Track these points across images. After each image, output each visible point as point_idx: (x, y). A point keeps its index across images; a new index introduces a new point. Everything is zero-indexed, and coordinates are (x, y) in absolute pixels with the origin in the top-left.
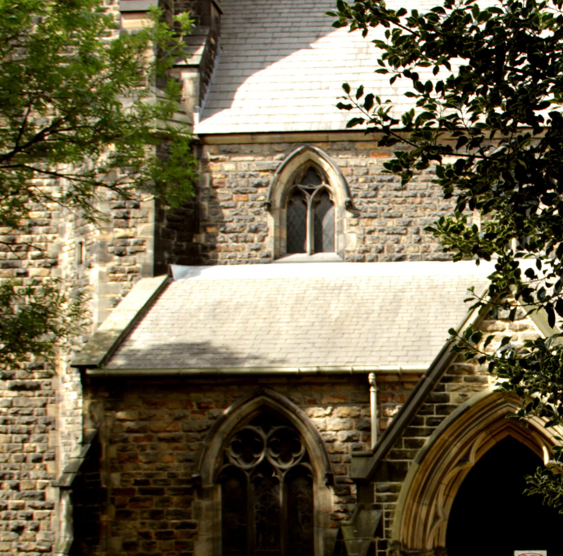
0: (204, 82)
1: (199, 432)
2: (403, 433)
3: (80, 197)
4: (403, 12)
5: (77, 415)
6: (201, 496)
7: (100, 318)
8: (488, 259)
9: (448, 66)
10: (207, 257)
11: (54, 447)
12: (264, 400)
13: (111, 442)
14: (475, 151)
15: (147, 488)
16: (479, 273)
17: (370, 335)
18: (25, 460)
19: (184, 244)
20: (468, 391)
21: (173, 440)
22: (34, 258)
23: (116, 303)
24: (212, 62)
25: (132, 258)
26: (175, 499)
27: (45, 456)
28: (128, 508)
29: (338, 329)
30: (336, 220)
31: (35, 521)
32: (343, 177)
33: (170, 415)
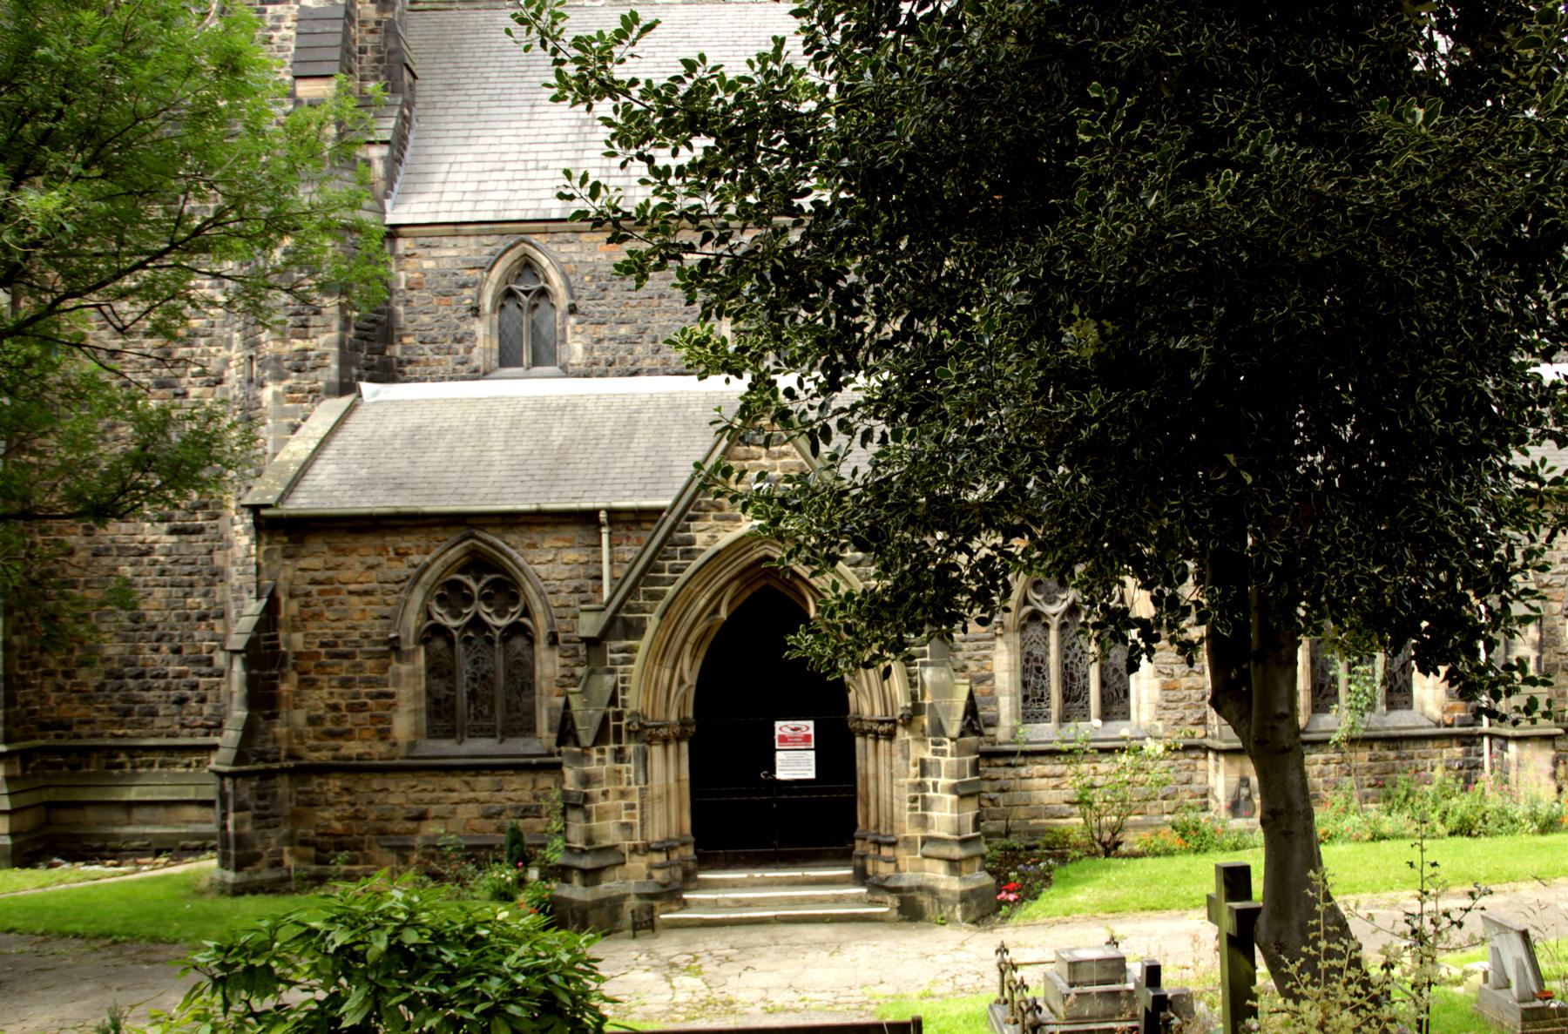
0: (394, 162)
3: (251, 299)
4: (634, 82)
6: (399, 660)
7: (275, 447)
8: (740, 376)
9: (690, 147)
10: (404, 373)
11: (222, 603)
13: (292, 596)
14: (722, 249)
15: (336, 651)
16: (731, 389)
18: (187, 618)
21: (366, 593)
22: (194, 376)
23: (295, 429)
24: (405, 138)
25: (313, 375)
26: (370, 663)
27: (212, 613)
28: (312, 675)
29: (562, 457)
30: (559, 327)
31: (201, 690)
32: (564, 275)
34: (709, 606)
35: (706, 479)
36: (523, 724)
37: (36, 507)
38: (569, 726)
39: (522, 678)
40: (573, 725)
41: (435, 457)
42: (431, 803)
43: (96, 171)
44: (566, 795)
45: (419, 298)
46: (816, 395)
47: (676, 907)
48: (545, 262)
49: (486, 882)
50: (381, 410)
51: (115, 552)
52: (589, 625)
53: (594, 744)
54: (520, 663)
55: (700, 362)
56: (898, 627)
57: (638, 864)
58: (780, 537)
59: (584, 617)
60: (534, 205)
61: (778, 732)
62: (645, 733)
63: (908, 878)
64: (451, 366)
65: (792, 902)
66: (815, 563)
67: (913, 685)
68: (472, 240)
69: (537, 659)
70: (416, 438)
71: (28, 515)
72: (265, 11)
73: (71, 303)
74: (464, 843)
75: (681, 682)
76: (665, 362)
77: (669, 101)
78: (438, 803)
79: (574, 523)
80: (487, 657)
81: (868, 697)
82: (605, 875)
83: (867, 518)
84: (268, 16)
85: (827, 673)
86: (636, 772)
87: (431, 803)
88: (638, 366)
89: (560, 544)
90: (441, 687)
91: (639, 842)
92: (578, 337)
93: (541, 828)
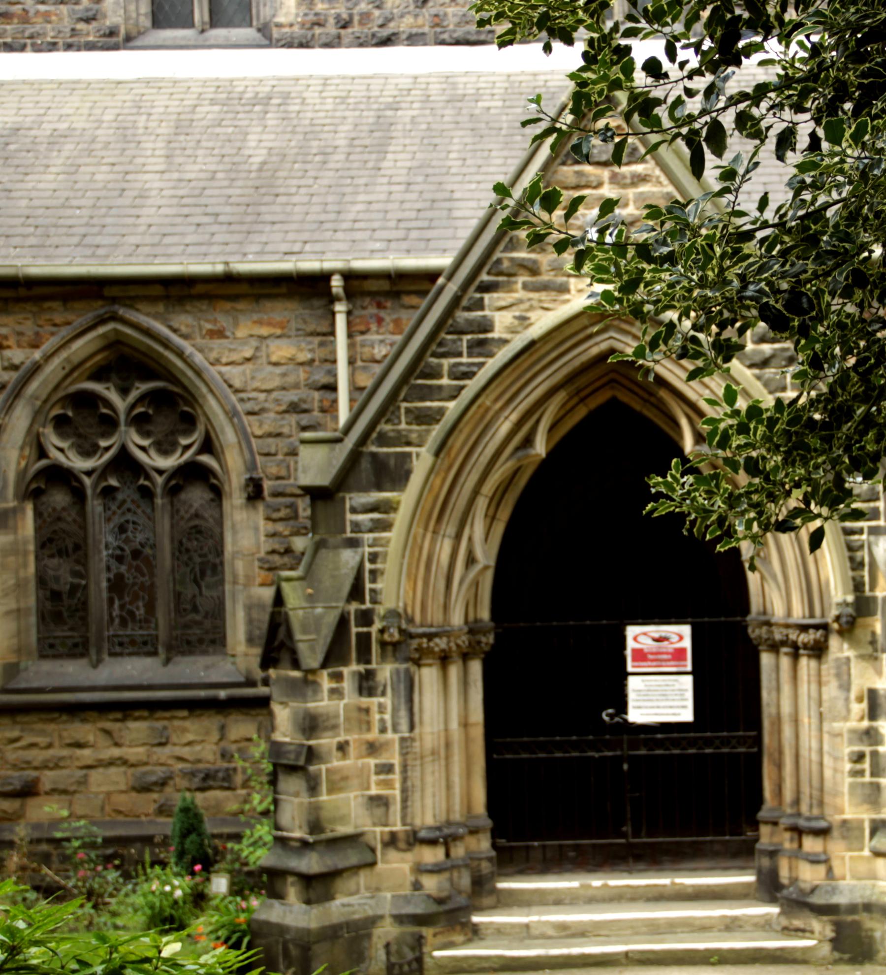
2: (402, 395)
8: (569, 41)
17: (330, 199)
20: (531, 308)
29: (266, 184)
34: (517, 434)
35: (516, 213)
36: (202, 632)
38: (282, 633)
39: (202, 554)
40: (289, 634)
41: (47, 181)
42: (45, 766)
44: (276, 749)
46: (698, 72)
47: (459, 938)
49: (138, 900)
52: (316, 466)
53: (324, 666)
54: (198, 530)
55: (500, 16)
56: (836, 462)
57: (397, 866)
58: (637, 312)
59: (305, 452)
61: (631, 644)
62: (411, 646)
63: (849, 889)
64: (67, 24)
65: (655, 929)
66: (697, 355)
67: (857, 565)
69: (227, 524)
74: (100, 834)
75: (471, 560)
76: (438, 21)
78: (57, 767)
79: (288, 296)
80: (142, 520)
81: (787, 577)
82: (341, 884)
83: (783, 275)
85: (718, 540)
86: (395, 710)
87: (45, 766)
88: (392, 27)
89: (264, 331)
90: (63, 572)
91: (398, 827)
93: (234, 807)
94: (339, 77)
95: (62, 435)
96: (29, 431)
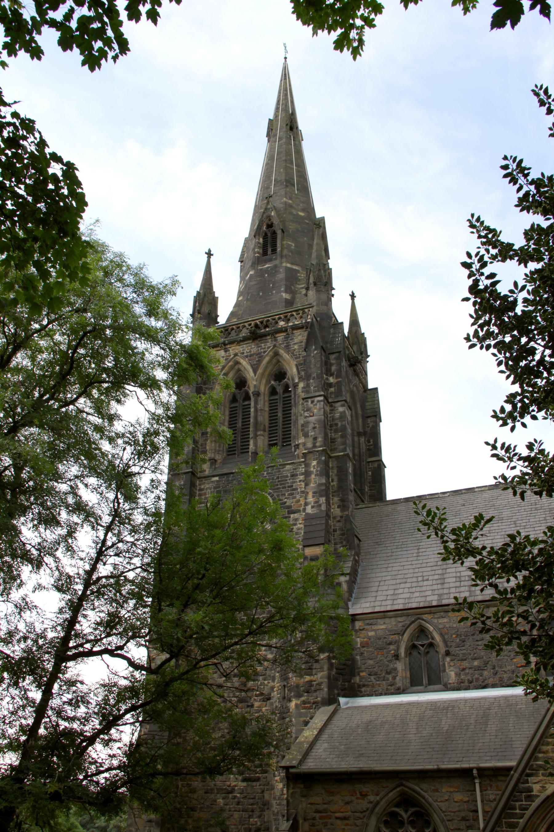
0: (352, 583)
1: (361, 812)
2: (503, 816)
4: (484, 548)
5: (283, 799)
9: (516, 577)
10: (361, 692)
11: (268, 822)
12: (403, 790)
13: (305, 819)
17: (470, 742)
19: (346, 683)
20: (546, 783)
21: (345, 818)
23: (306, 723)
25: (315, 694)
30: (441, 663)
32: (441, 635)
33: (343, 800)
37: (183, 768)
43: (218, 600)
45: (367, 652)
48: (431, 628)
50: (350, 712)
51: (216, 791)
60: (423, 599)
64: (385, 687)
68: (393, 619)
70: (369, 728)
71: (178, 773)
72: (290, 517)
73: (202, 663)
76: (501, 679)
77: (503, 556)
84: (291, 519)
89: (452, 790)
92: (452, 668)
94: (477, 488)
95: (387, 827)
96: (376, 826)
